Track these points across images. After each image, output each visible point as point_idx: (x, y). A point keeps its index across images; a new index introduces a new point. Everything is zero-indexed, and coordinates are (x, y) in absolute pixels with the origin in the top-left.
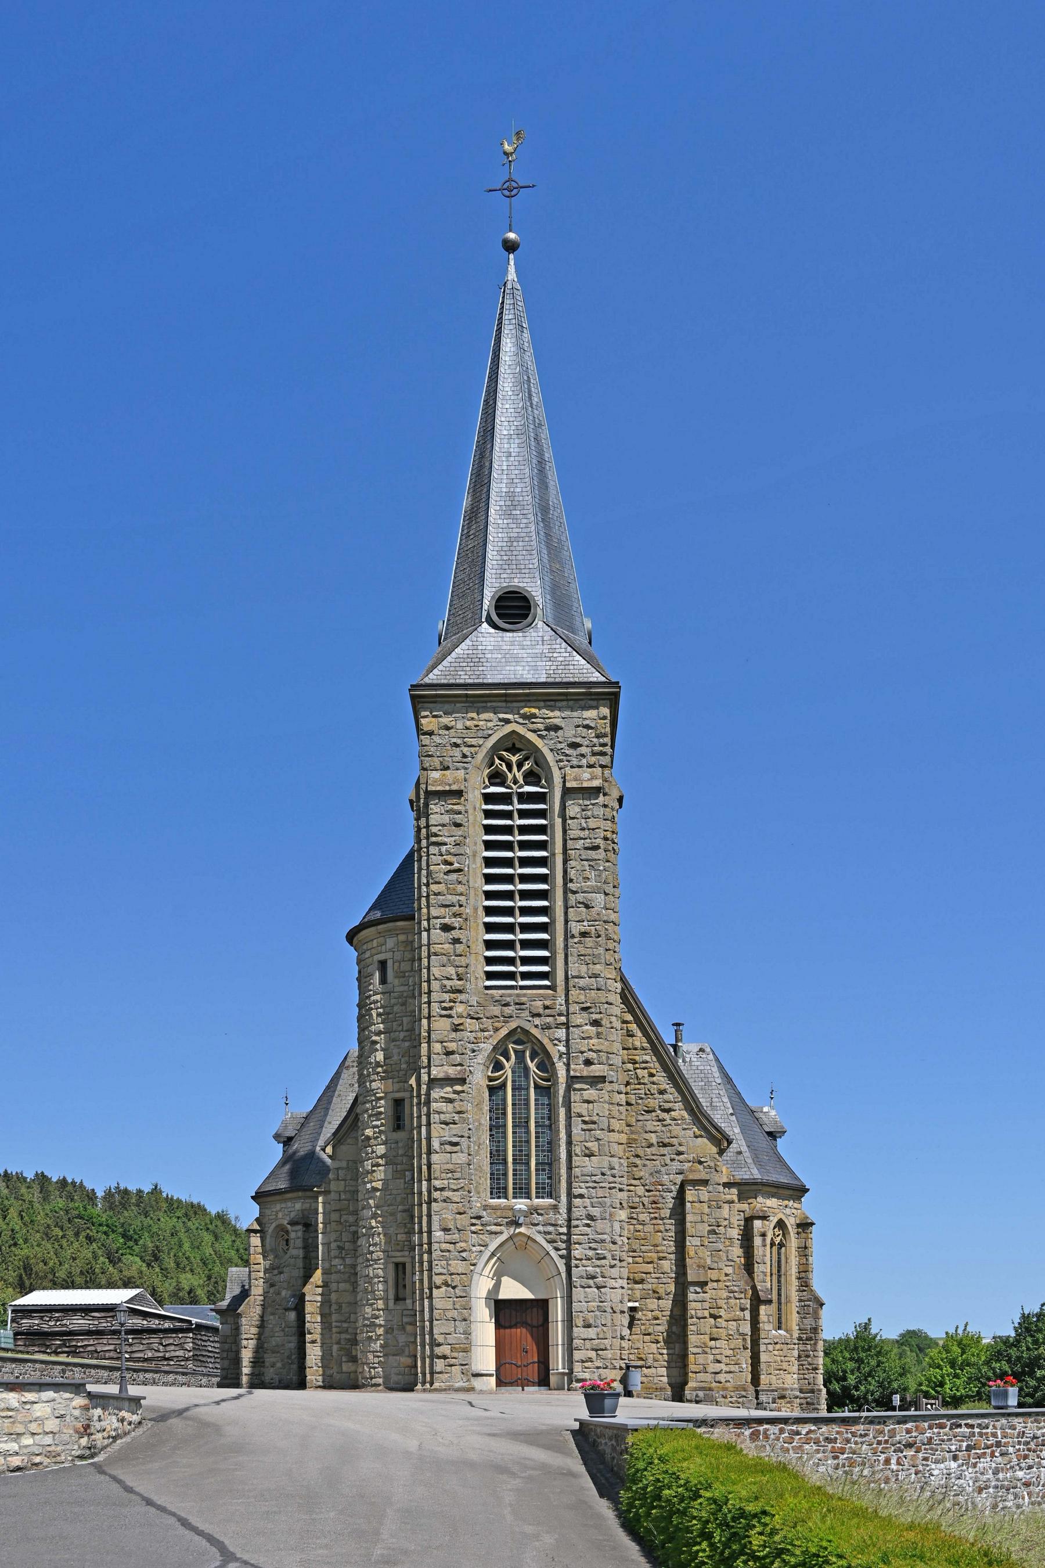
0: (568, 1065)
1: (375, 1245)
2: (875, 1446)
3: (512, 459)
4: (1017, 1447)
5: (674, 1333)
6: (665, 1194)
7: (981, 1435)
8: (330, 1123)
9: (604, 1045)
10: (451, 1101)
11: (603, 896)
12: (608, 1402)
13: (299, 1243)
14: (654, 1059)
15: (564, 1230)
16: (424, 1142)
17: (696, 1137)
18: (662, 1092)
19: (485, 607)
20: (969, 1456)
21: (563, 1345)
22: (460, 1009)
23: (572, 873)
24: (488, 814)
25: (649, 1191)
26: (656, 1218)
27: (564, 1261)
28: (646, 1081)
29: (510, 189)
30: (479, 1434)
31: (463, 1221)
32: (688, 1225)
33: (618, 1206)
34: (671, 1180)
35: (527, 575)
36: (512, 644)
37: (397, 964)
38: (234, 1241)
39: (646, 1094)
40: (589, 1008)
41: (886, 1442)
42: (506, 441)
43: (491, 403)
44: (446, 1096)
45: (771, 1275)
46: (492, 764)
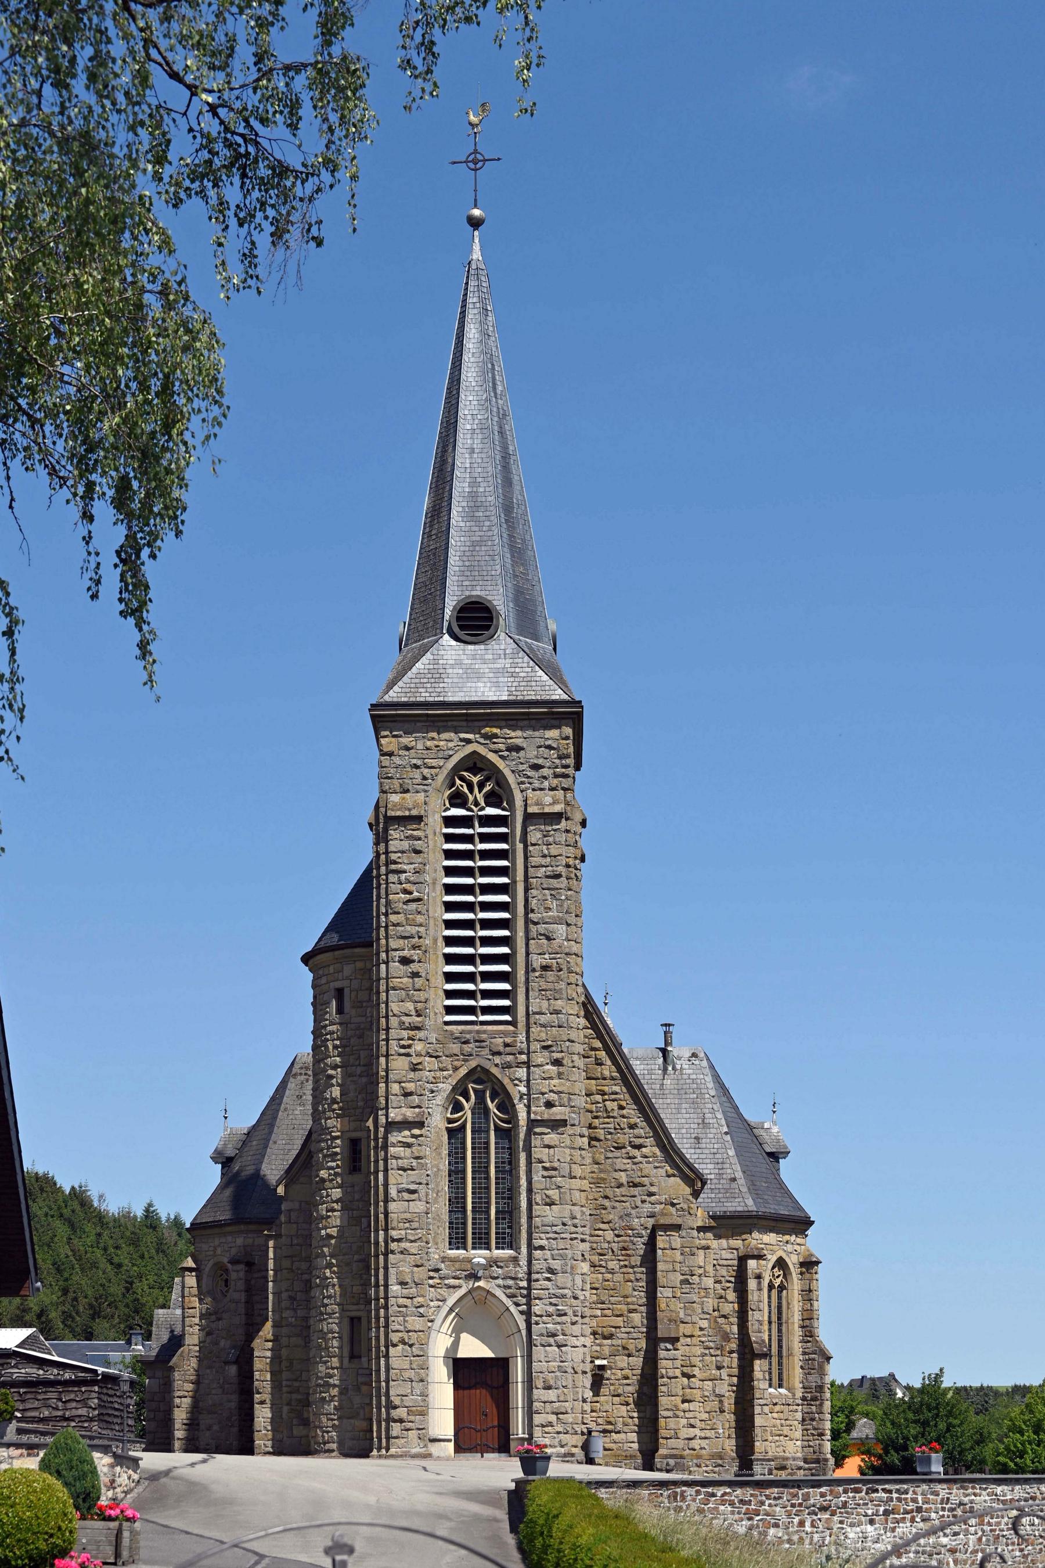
0: (528, 1107)
1: (329, 1297)
2: (789, 1508)
3: (475, 456)
4: (941, 1513)
5: (645, 1394)
6: (635, 1239)
7: (899, 1500)
8: (275, 1143)
10: (409, 1145)
11: (564, 927)
13: (241, 1285)
14: (624, 1090)
15: (524, 1284)
17: (669, 1176)
18: (632, 1127)
19: (447, 617)
20: (886, 1521)
21: (523, 1408)
22: (419, 1047)
23: (533, 903)
25: (618, 1236)
26: (626, 1266)
27: (524, 1317)
28: (615, 1114)
29: (475, 162)
30: (428, 1492)
31: (420, 1274)
32: (659, 1274)
33: (580, 1258)
34: (641, 1223)
35: (489, 583)
37: (354, 994)
38: (99, 1235)
39: (615, 1129)
40: (550, 1046)
41: (800, 1505)
42: (469, 436)
43: (455, 392)
44: (404, 1140)
45: (770, 1323)
46: (453, 784)
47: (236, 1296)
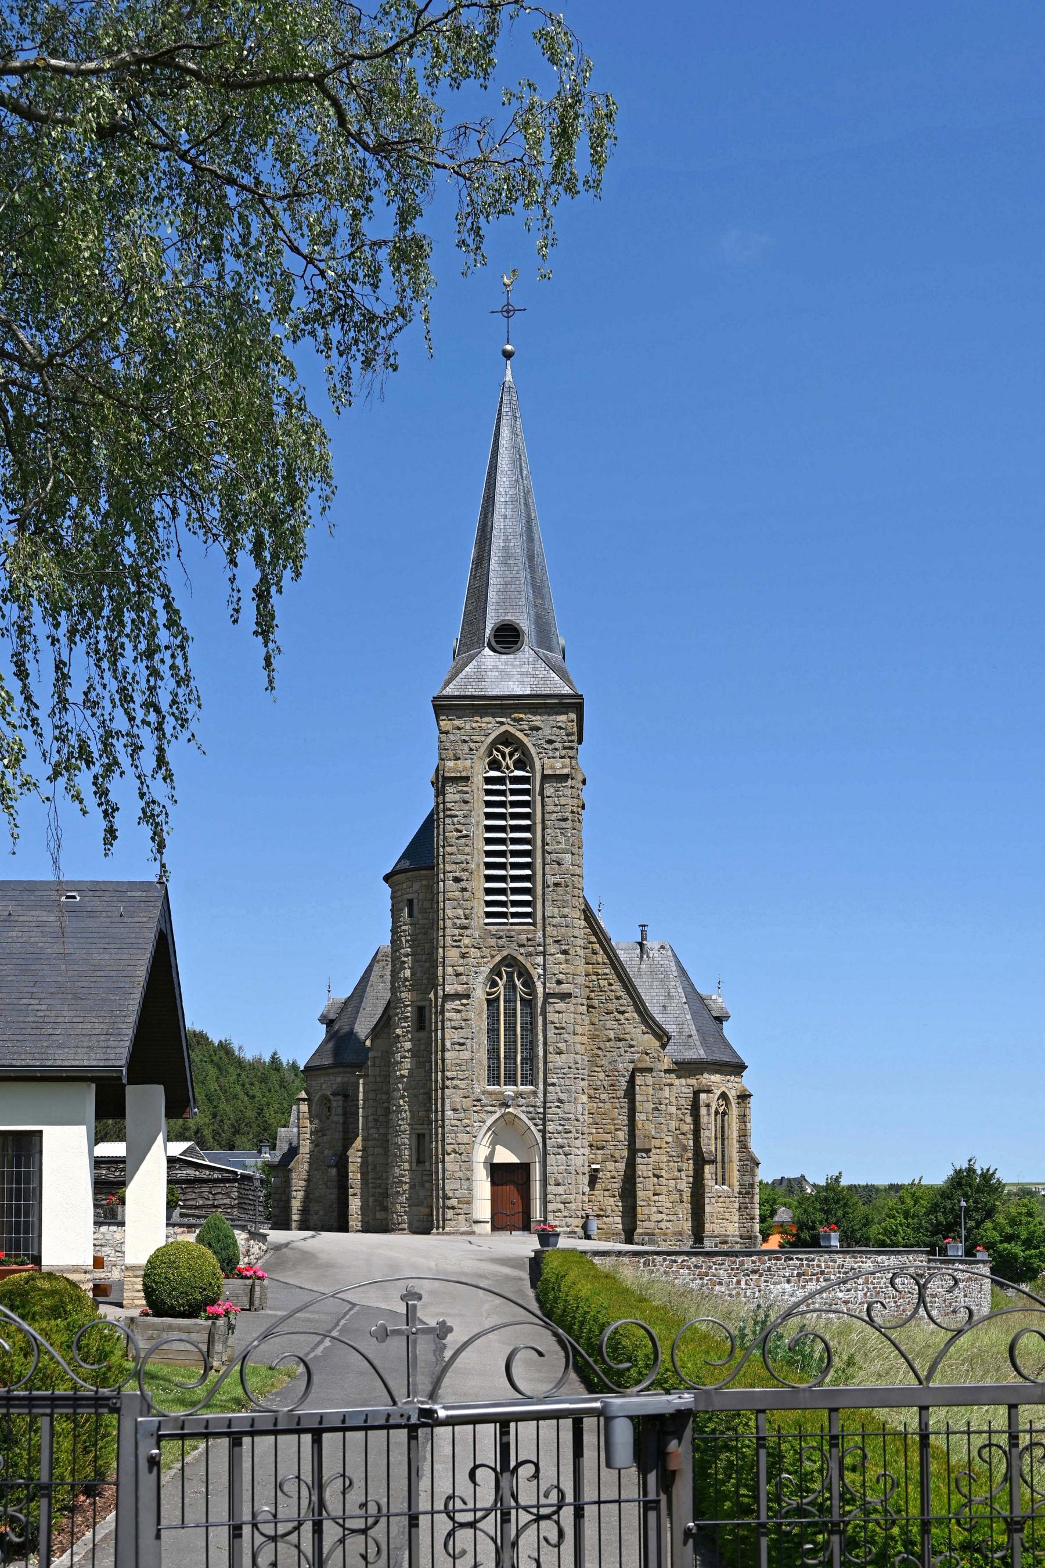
0: (544, 984)
1: (403, 1119)
9: (570, 969)
10: (459, 1011)
12: (552, 1239)
13: (340, 1111)
15: (541, 1110)
16: (439, 1042)
18: (618, 998)
19: (487, 635)
22: (466, 941)
23: (548, 838)
24: (488, 792)
29: (508, 311)
31: (468, 1103)
32: (637, 1103)
34: (624, 1067)
36: (506, 664)
41: (738, 1269)
45: (716, 1138)
46: (491, 754)
47: (336, 1118)
